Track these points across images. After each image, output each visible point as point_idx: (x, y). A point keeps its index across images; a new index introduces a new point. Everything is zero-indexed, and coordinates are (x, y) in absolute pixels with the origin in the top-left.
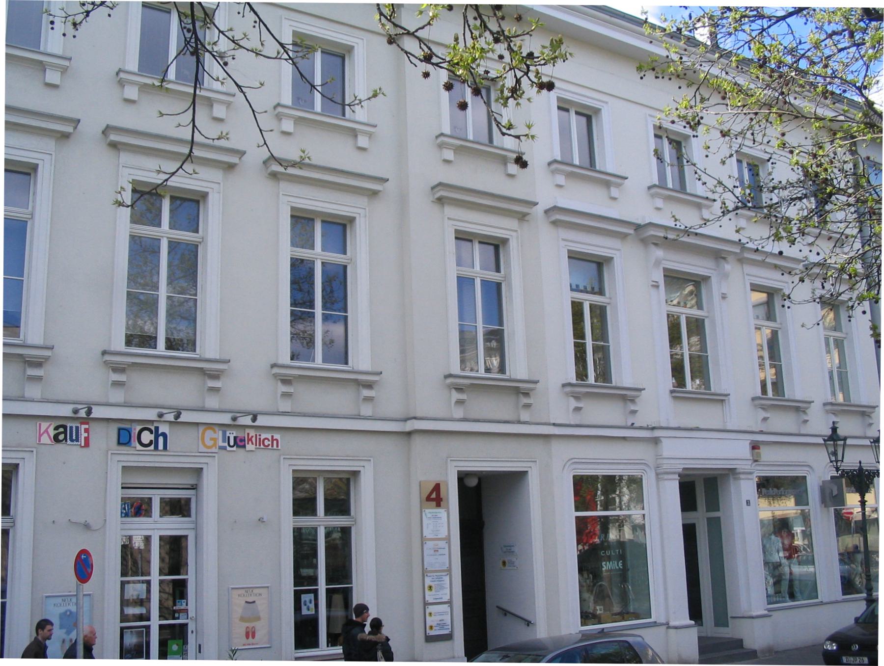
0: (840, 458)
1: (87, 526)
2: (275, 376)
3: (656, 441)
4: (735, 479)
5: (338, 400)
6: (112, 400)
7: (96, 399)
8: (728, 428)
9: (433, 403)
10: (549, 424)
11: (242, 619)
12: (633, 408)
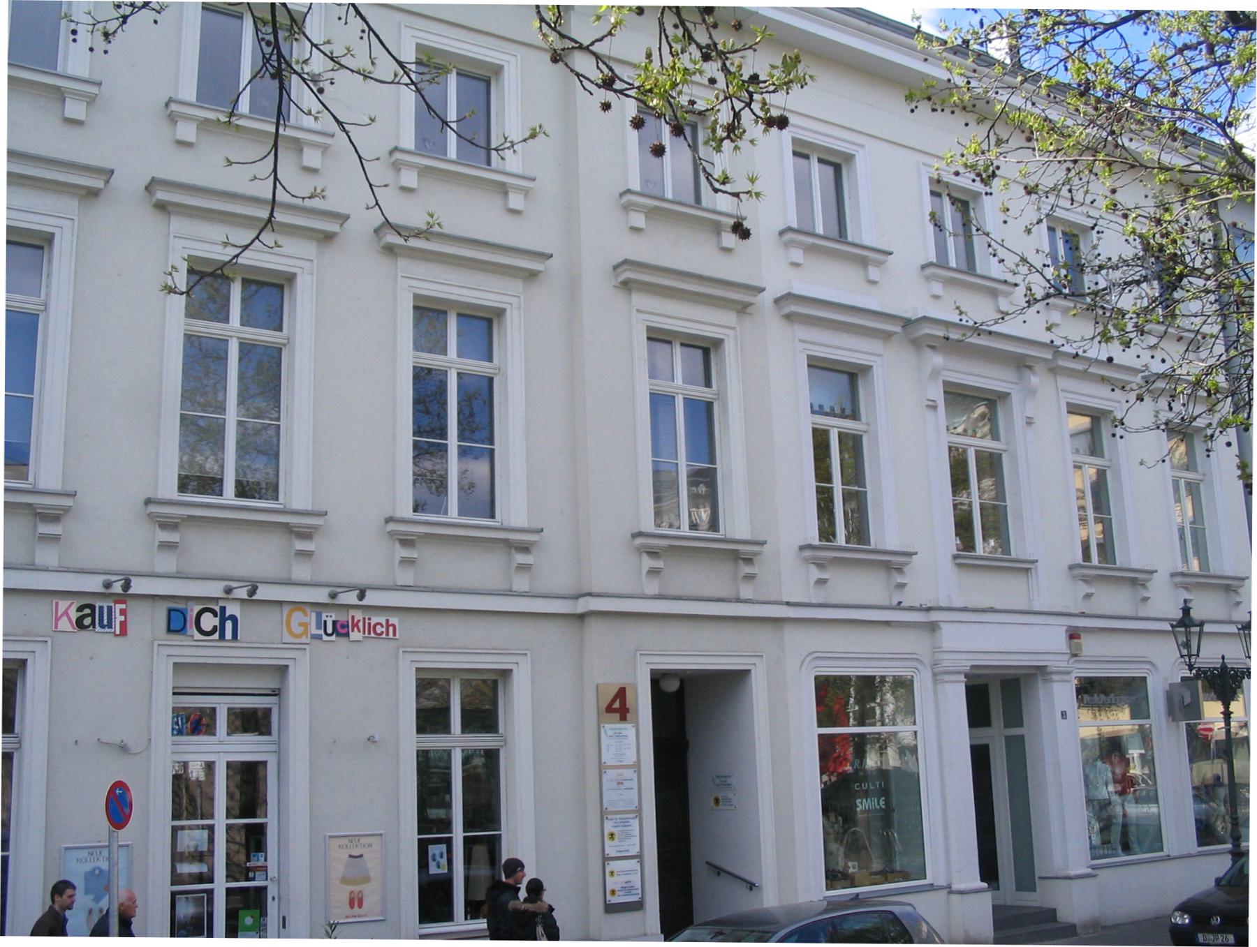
0: (1194, 651)
1: (123, 748)
2: (391, 534)
3: (933, 627)
4: (1045, 681)
5: (481, 569)
6: (159, 569)
7: (136, 567)
8: (1036, 609)
9: (616, 573)
10: (781, 603)
11: (344, 880)
12: (900, 580)
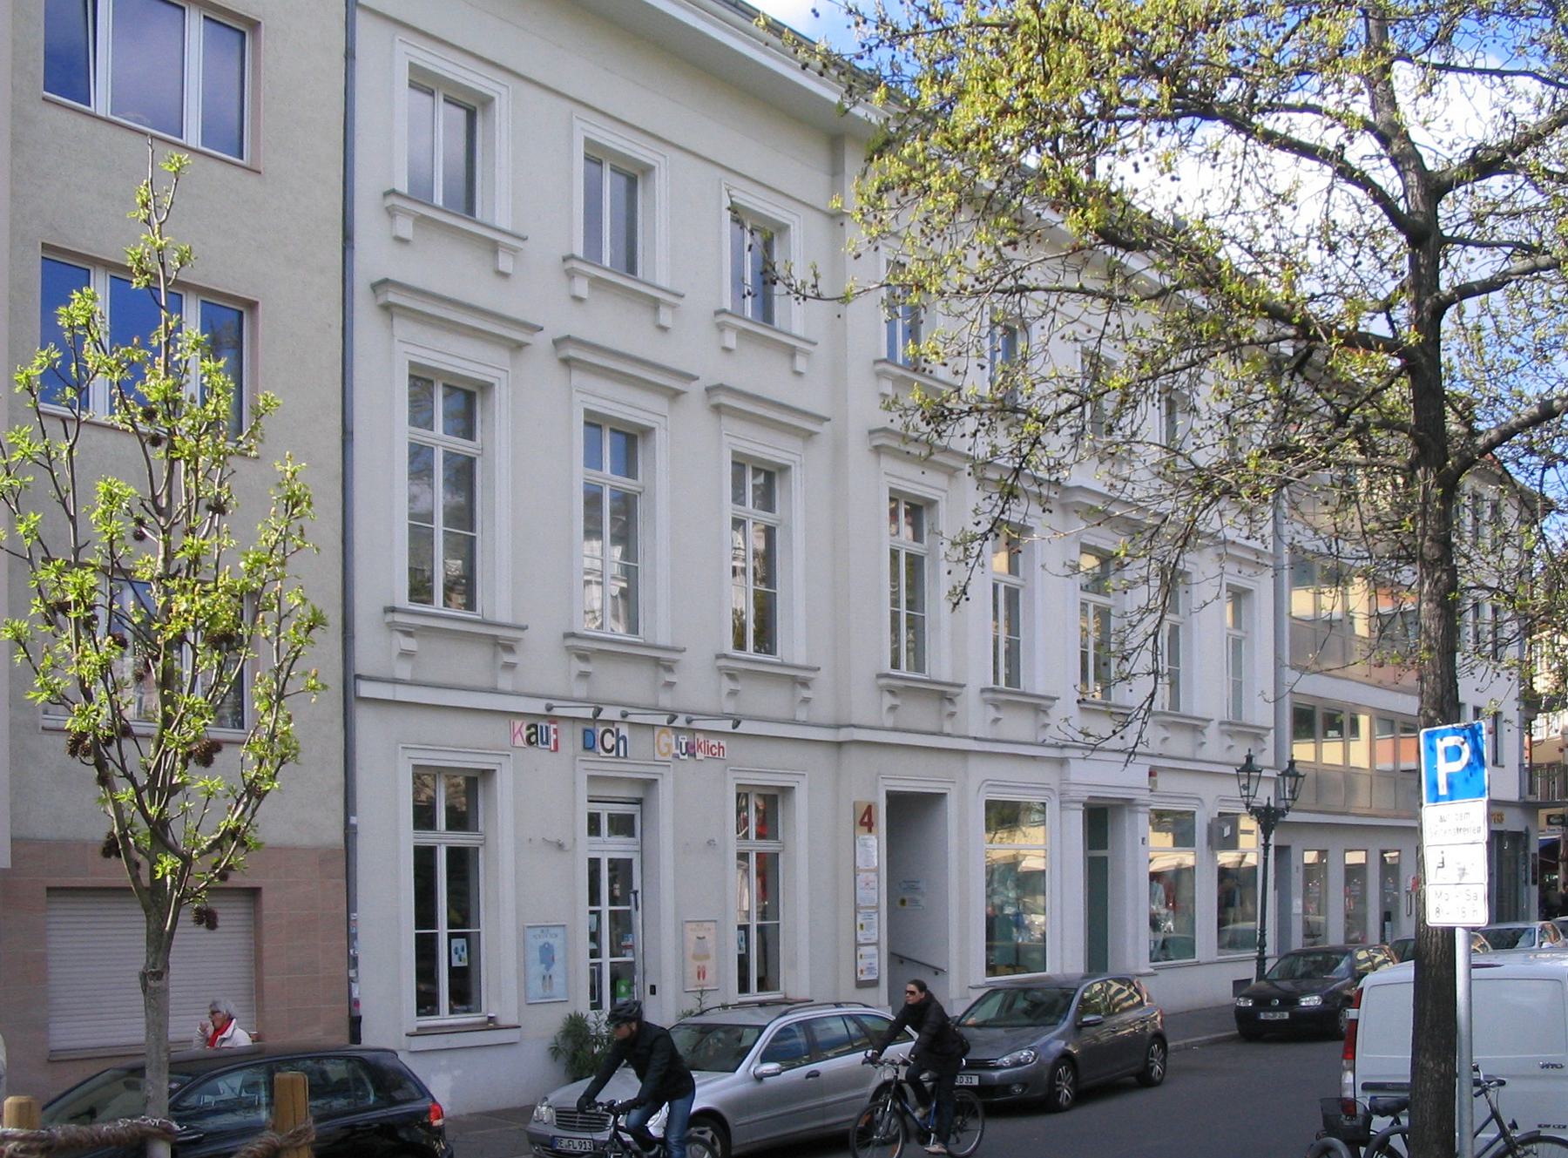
1: (560, 846)
2: (720, 669)
3: (1063, 762)
4: (1131, 811)
5: (470, 663)
6: (576, 695)
7: (698, 707)
9: (868, 708)
11: (695, 957)
12: (669, 678)
